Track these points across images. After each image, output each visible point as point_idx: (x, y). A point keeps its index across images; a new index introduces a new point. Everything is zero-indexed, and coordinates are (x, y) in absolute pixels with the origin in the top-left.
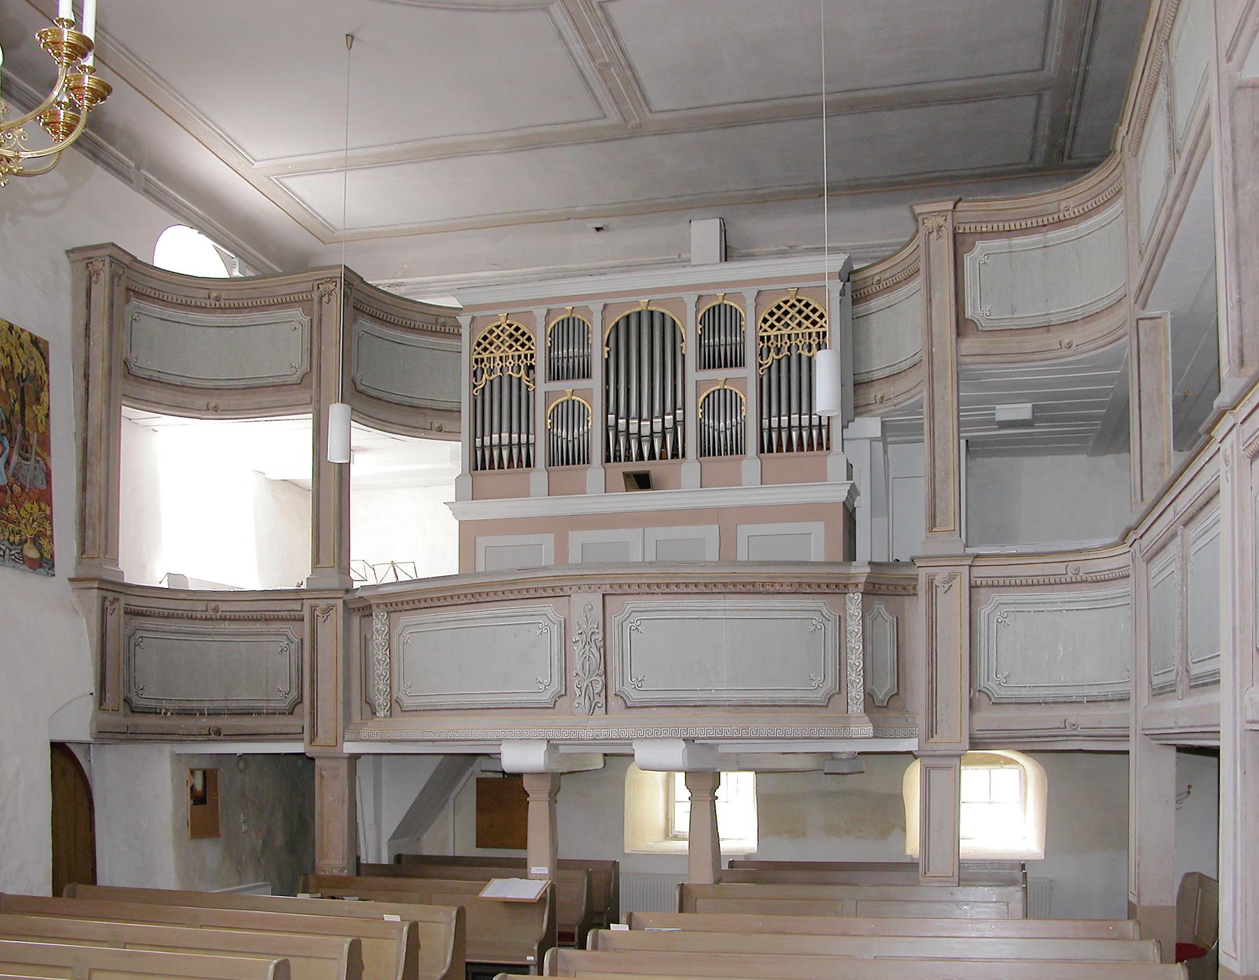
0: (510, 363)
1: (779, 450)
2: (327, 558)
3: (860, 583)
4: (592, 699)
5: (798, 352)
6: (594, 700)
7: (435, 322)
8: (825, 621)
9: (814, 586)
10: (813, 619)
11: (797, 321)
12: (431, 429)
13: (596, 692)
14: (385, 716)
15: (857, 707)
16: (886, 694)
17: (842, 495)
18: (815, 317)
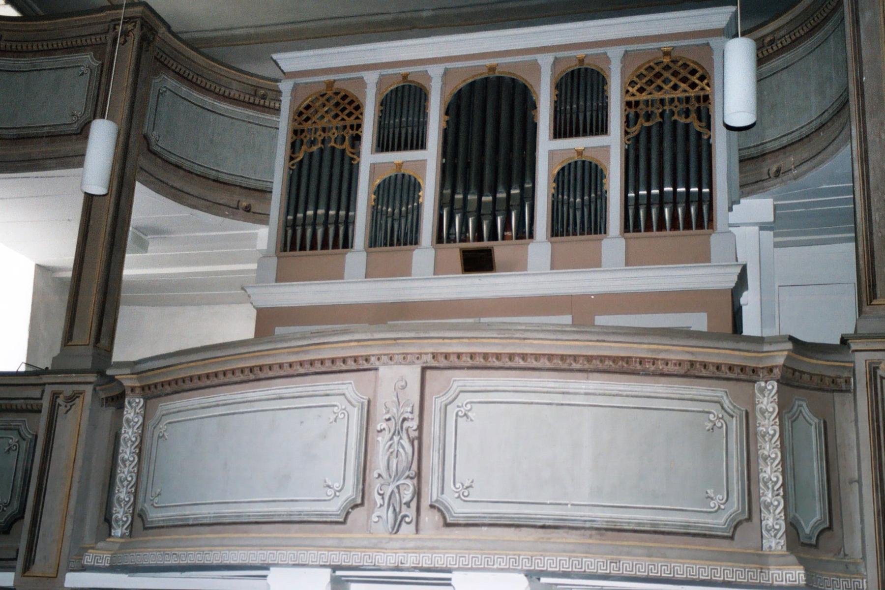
0: (334, 134)
1: (649, 228)
2: (84, 334)
3: (776, 367)
4: (398, 510)
5: (673, 118)
6: (400, 512)
7: (253, 93)
8: (727, 417)
9: (711, 368)
10: (709, 413)
11: (672, 84)
12: (237, 208)
13: (404, 501)
14: (123, 536)
15: (775, 543)
16: (815, 527)
17: (730, 280)
18: (695, 79)
